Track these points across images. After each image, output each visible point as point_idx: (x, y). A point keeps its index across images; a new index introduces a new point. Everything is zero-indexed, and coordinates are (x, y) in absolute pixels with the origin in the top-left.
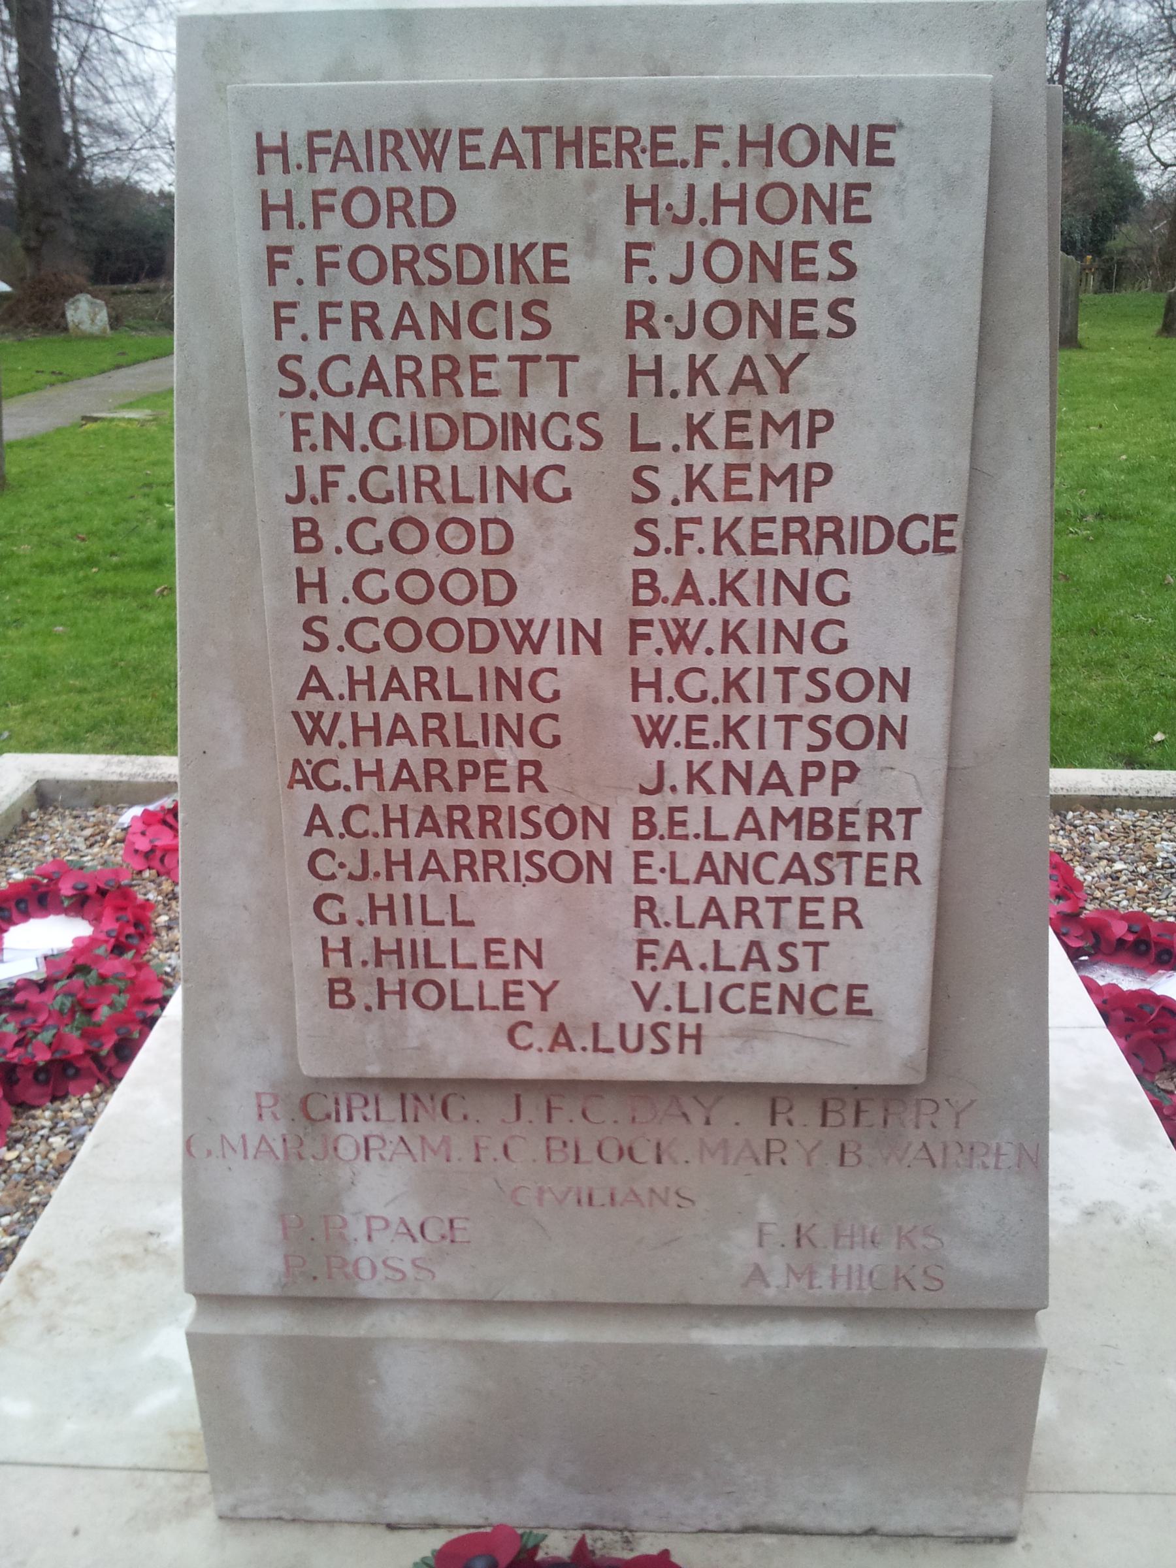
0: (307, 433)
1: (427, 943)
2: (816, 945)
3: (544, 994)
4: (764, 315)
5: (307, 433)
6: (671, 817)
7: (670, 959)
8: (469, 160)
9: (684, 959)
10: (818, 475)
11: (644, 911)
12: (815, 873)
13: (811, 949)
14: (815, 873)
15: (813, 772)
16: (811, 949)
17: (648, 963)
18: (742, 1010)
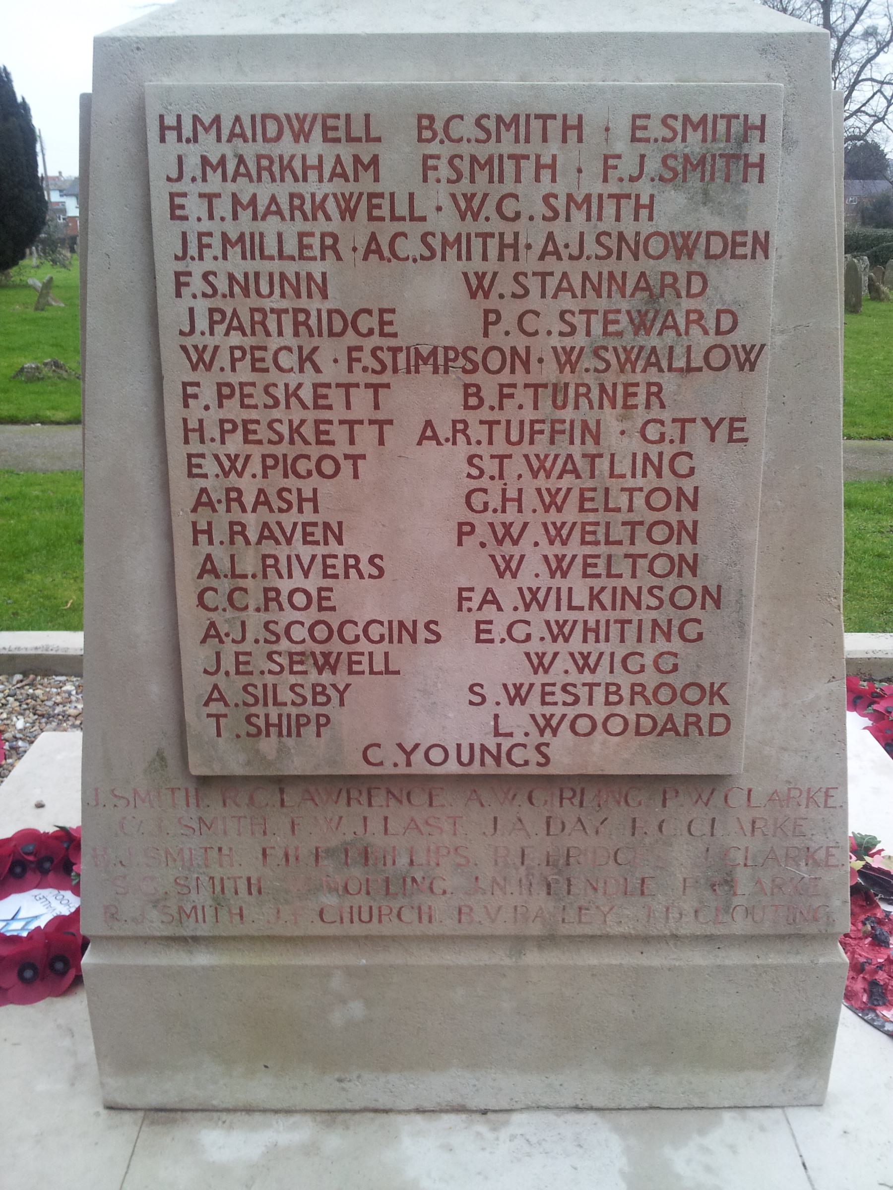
0: (209, 246)
1: (275, 686)
2: (376, 387)
3: (342, 694)
4: (238, 283)
5: (209, 246)
6: (200, 240)
7: (484, 601)
8: (318, 701)
9: (495, 601)
10: (323, 720)
11: (238, 533)
12: (276, 503)
13: (346, 427)
14: (276, 503)
15: (270, 462)
16: (346, 427)
17: (466, 605)
18: (291, 370)
